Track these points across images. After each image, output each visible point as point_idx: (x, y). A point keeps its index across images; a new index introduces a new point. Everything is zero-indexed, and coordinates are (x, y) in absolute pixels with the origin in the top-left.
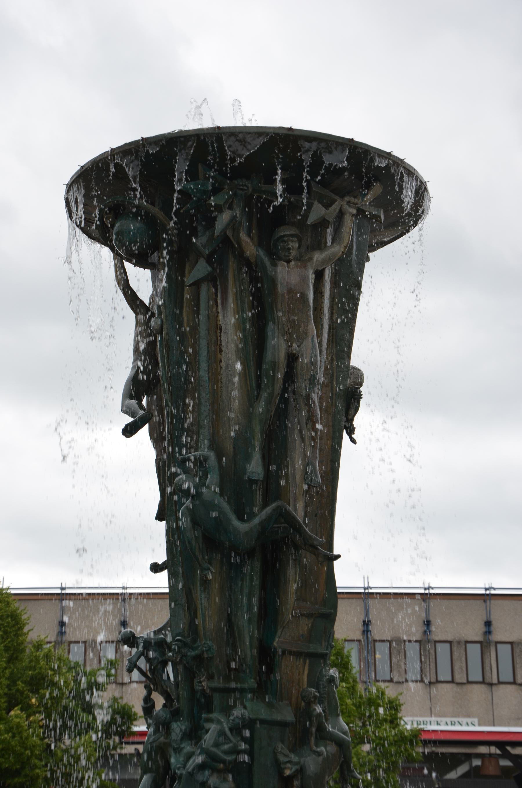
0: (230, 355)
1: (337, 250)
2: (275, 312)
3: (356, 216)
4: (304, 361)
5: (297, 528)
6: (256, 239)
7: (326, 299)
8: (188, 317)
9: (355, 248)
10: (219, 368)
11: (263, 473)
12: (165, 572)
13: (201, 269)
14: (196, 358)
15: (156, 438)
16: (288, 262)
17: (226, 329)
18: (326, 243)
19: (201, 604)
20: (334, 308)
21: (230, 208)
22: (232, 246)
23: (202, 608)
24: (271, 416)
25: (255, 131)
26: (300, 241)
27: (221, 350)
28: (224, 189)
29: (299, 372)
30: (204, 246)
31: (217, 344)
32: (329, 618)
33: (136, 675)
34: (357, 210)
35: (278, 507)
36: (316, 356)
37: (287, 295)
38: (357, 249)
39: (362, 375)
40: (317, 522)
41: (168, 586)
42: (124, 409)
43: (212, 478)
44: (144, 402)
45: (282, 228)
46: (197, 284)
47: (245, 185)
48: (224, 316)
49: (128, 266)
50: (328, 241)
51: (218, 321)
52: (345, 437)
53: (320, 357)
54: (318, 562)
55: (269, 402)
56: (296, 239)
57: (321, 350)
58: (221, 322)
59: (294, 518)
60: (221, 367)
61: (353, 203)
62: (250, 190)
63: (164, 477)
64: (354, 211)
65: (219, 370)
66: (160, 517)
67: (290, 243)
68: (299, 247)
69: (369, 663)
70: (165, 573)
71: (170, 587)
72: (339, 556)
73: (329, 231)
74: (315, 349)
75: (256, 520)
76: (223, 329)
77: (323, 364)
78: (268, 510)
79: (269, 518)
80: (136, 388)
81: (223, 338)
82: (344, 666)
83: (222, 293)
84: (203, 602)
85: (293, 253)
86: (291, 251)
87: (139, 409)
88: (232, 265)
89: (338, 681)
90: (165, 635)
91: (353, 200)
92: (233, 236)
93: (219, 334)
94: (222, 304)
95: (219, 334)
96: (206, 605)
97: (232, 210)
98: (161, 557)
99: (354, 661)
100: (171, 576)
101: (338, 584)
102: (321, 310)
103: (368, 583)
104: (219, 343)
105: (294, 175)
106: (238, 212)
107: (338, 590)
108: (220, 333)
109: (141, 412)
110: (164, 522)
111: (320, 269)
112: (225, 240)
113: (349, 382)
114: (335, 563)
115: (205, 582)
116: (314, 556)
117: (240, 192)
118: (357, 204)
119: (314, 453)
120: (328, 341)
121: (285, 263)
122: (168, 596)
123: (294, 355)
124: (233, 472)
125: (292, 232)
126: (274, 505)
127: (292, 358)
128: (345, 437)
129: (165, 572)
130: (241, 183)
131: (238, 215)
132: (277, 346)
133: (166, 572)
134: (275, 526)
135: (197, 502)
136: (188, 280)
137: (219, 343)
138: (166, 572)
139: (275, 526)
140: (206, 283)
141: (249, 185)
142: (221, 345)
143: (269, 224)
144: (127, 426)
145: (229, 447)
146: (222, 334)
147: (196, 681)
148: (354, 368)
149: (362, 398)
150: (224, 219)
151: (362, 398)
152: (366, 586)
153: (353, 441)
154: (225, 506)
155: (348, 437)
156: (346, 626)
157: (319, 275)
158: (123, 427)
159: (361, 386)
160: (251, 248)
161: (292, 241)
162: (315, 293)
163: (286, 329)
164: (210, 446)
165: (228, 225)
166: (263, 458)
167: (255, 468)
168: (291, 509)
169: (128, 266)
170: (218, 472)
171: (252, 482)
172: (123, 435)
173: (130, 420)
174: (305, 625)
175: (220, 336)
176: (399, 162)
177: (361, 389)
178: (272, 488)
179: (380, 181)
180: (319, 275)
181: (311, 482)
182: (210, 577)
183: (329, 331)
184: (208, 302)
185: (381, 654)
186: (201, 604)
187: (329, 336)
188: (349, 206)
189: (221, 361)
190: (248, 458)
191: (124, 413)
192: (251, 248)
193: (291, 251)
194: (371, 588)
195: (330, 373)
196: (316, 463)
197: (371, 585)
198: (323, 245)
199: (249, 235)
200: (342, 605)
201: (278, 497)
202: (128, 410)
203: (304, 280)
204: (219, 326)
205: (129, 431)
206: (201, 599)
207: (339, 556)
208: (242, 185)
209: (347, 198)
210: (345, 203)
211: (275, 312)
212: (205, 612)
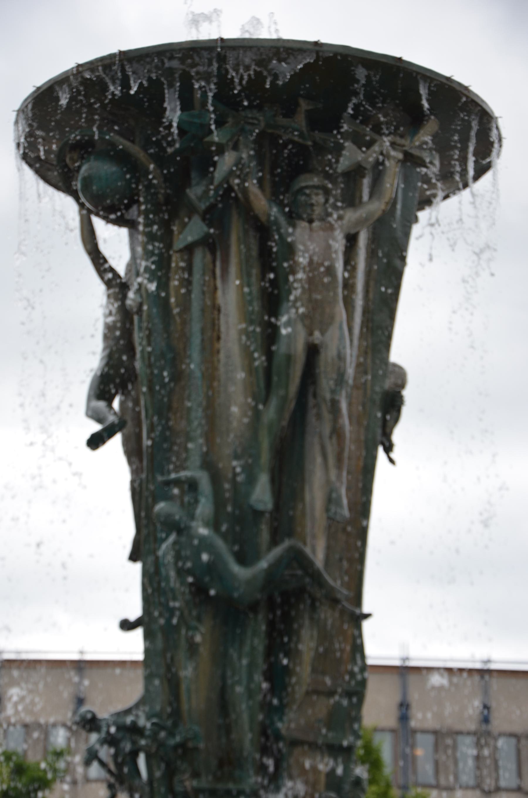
1: (375, 207)
4: (328, 355)
5: (316, 577)
6: (268, 190)
9: (399, 206)
13: (193, 230)
15: (133, 452)
18: (361, 197)
21: (235, 147)
25: (178, 47)
27: (219, 338)
28: (227, 122)
29: (322, 369)
30: (200, 199)
32: (357, 693)
33: (95, 770)
36: (344, 348)
38: (404, 206)
43: (204, 507)
45: (302, 177)
49: (98, 223)
52: (381, 451)
55: (281, 409)
57: (351, 341)
58: (220, 299)
59: (311, 563)
63: (142, 498)
64: (400, 156)
66: (134, 557)
69: (407, 760)
70: (139, 633)
73: (366, 182)
75: (264, 564)
78: (277, 551)
80: (104, 388)
82: (374, 762)
85: (318, 210)
89: (365, 784)
90: (137, 716)
91: (398, 140)
98: (135, 610)
99: (386, 754)
100: (147, 636)
111: (353, 231)
113: (388, 384)
115: (193, 649)
119: (339, 476)
126: (287, 543)
127: (313, 351)
128: (381, 451)
130: (250, 115)
143: (289, 169)
147: (176, 779)
148: (395, 365)
150: (226, 162)
153: (392, 461)
154: (220, 543)
156: (377, 710)
157: (351, 240)
159: (403, 385)
161: (317, 194)
166: (273, 481)
167: (262, 495)
168: (308, 550)
169: (98, 223)
171: (258, 514)
173: (96, 427)
174: (321, 707)
178: (284, 520)
180: (351, 240)
182: (198, 639)
185: (422, 751)
192: (261, 203)
195: (361, 368)
198: (357, 201)
201: (290, 534)
205: (95, 442)
208: (252, 118)
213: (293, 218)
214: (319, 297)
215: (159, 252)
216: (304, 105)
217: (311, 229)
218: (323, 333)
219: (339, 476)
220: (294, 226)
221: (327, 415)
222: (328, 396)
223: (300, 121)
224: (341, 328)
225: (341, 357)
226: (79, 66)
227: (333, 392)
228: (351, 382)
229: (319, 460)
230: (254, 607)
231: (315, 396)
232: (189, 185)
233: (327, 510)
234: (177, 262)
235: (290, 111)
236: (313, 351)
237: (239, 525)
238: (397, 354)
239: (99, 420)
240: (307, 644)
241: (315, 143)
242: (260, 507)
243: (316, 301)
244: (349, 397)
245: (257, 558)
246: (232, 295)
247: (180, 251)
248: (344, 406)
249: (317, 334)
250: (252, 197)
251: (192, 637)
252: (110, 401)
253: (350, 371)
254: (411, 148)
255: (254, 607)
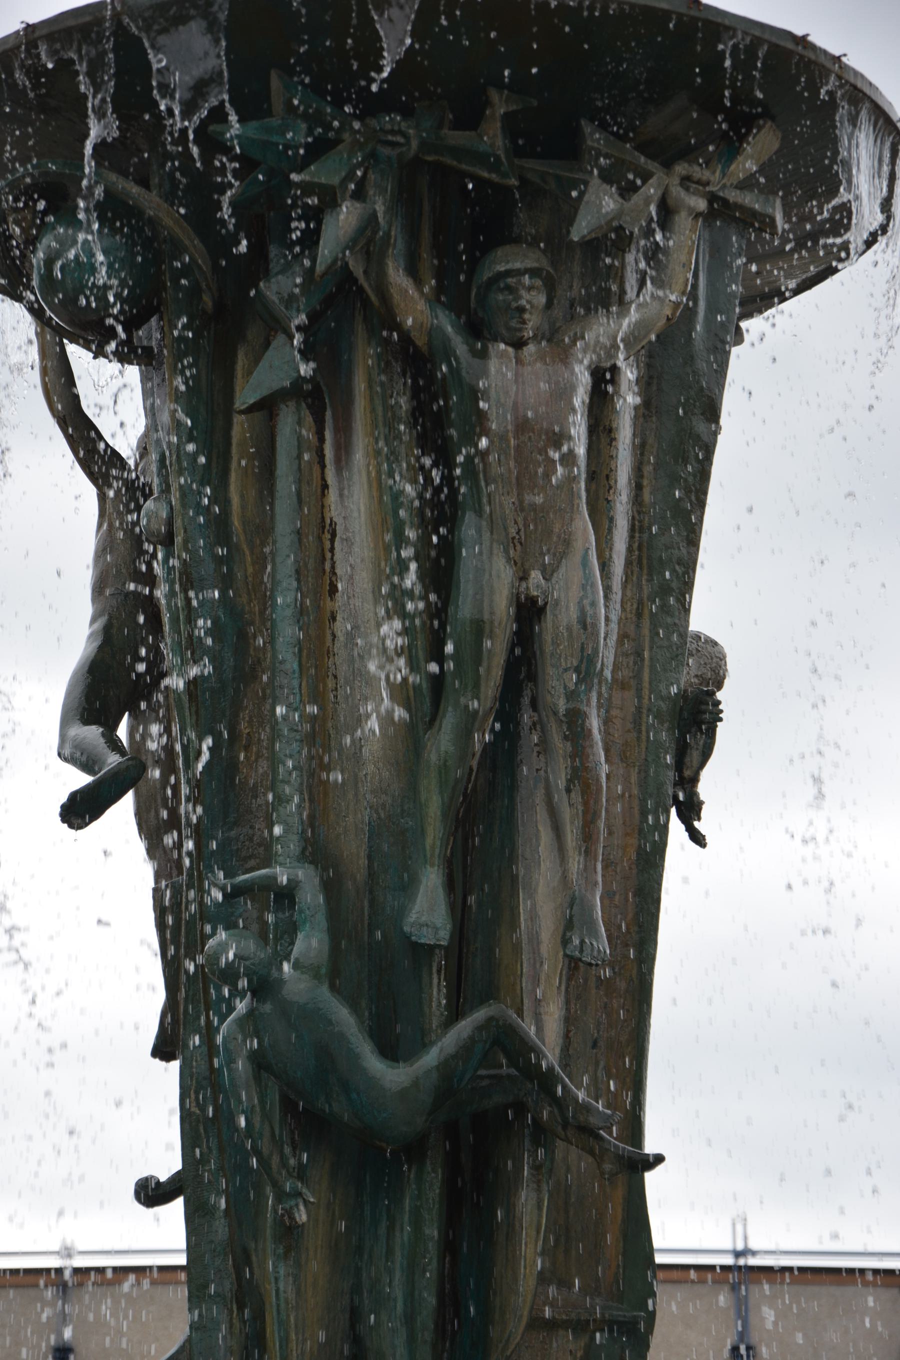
0: (358, 603)
2: (483, 484)
3: (709, 217)
5: (547, 1080)
7: (621, 447)
8: (242, 497)
10: (329, 637)
11: (449, 927)
12: (178, 1205)
14: (265, 609)
16: (518, 344)
17: (346, 529)
19: (277, 1291)
20: (645, 474)
21: (359, 195)
22: (366, 302)
23: (278, 1305)
24: (471, 769)
26: (550, 286)
27: (333, 590)
28: (343, 141)
29: (549, 649)
31: (324, 570)
34: (710, 203)
35: (490, 1019)
36: (594, 604)
37: (516, 437)
39: (722, 658)
40: (597, 1064)
41: (183, 1245)
42: (67, 752)
43: (310, 942)
44: (122, 732)
45: (500, 252)
46: (267, 406)
47: (401, 133)
48: (341, 495)
49: (77, 354)
50: (628, 290)
51: (326, 510)
52: (676, 827)
53: (606, 607)
54: (602, 1173)
56: (538, 283)
57: (608, 589)
58: (334, 512)
60: (334, 636)
61: (699, 182)
62: (414, 144)
63: (178, 930)
64: (702, 205)
65: (329, 642)
66: (164, 1049)
67: (523, 293)
68: (549, 305)
71: (191, 1249)
72: (659, 1159)
74: (593, 585)
75: (431, 1058)
76: (339, 530)
77: (614, 626)
79: (466, 1049)
80: (104, 691)
81: (338, 555)
83: (336, 430)
84: (281, 1286)
85: (533, 322)
86: (527, 316)
87: (107, 751)
88: (365, 359)
91: (698, 172)
92: (365, 272)
93: (328, 545)
94: (338, 461)
95: (328, 545)
96: (291, 1296)
97: (364, 201)
98: (167, 1163)
101: (658, 1240)
102: (607, 477)
103: (746, 1238)
104: (328, 566)
105: (535, 103)
106: (380, 208)
107: (659, 1259)
108: (332, 541)
109: (113, 759)
110: (176, 1065)
112: (343, 277)
113: (687, 676)
114: (651, 1178)
115: (289, 1233)
116: (591, 1159)
117: (385, 151)
118: (708, 183)
119: (588, 870)
120: (628, 563)
121: (510, 350)
122: (183, 1276)
123: (533, 600)
124: (366, 922)
125: (530, 264)
126: (480, 1015)
127: (529, 612)
128: (676, 827)
129: (178, 1205)
131: (380, 216)
132: (490, 581)
133: (180, 1202)
134: (482, 1072)
135: (267, 1008)
136: (246, 395)
137: (328, 566)
138: (180, 1202)
139: (482, 1072)
140: (292, 404)
141: (411, 131)
142: (335, 574)
144: (73, 796)
145: (353, 850)
146: (336, 544)
148: (697, 636)
149: (721, 720)
151: (721, 720)
152: (740, 1246)
153: (698, 838)
155: (682, 827)
157: (603, 379)
158: (64, 799)
159: (719, 685)
160: (415, 306)
161: (530, 289)
162: (593, 430)
163: (513, 531)
164: (304, 850)
165: (352, 244)
166: (450, 885)
167: (428, 912)
169: (77, 354)
170: (324, 924)
171: (421, 953)
172: (63, 821)
173: (81, 779)
175: (332, 550)
176: (828, 64)
177: (719, 695)
178: (475, 960)
179: (773, 118)
180: (603, 379)
181: (581, 951)
182: (302, 1216)
183: (631, 537)
184: (299, 457)
186: (277, 1291)
187: (630, 550)
188: (687, 189)
189: (333, 618)
190: (408, 887)
191: (66, 760)
193: (527, 316)
194: (754, 1253)
196: (594, 896)
197: (753, 1245)
199: (413, 271)
200: (668, 1304)
201: (489, 994)
202: (79, 754)
203: (564, 393)
204: (328, 522)
205: (80, 810)
206: (276, 1279)
207: (659, 1159)
208: (392, 132)
209: (681, 169)
210: (676, 181)
211: (483, 484)
212: (288, 1316)
213: (478, 330)
214: (539, 500)
215: (205, 403)
216: (500, 106)
217: (519, 361)
218: (548, 573)
219: (588, 870)
220: (483, 355)
221: (560, 745)
222: (562, 705)
223: (492, 137)
224: (585, 562)
225: (586, 624)
226: (30, 28)
227: (571, 695)
228: (608, 674)
229: (546, 836)
230: (415, 1150)
231: (534, 705)
232: (266, 274)
233: (566, 942)
234: (240, 427)
235: (471, 117)
236: (529, 612)
237: (381, 976)
238: (705, 615)
239: (87, 767)
240: (529, 1208)
241: (524, 182)
242: (427, 938)
243: (533, 507)
244: (606, 706)
245: (424, 1045)
246: (361, 495)
247: (250, 410)
248: (595, 724)
249: (536, 576)
250: (396, 298)
251: (290, 1213)
252: (111, 727)
253: (607, 655)
254: (724, 187)
255: (415, 1150)
